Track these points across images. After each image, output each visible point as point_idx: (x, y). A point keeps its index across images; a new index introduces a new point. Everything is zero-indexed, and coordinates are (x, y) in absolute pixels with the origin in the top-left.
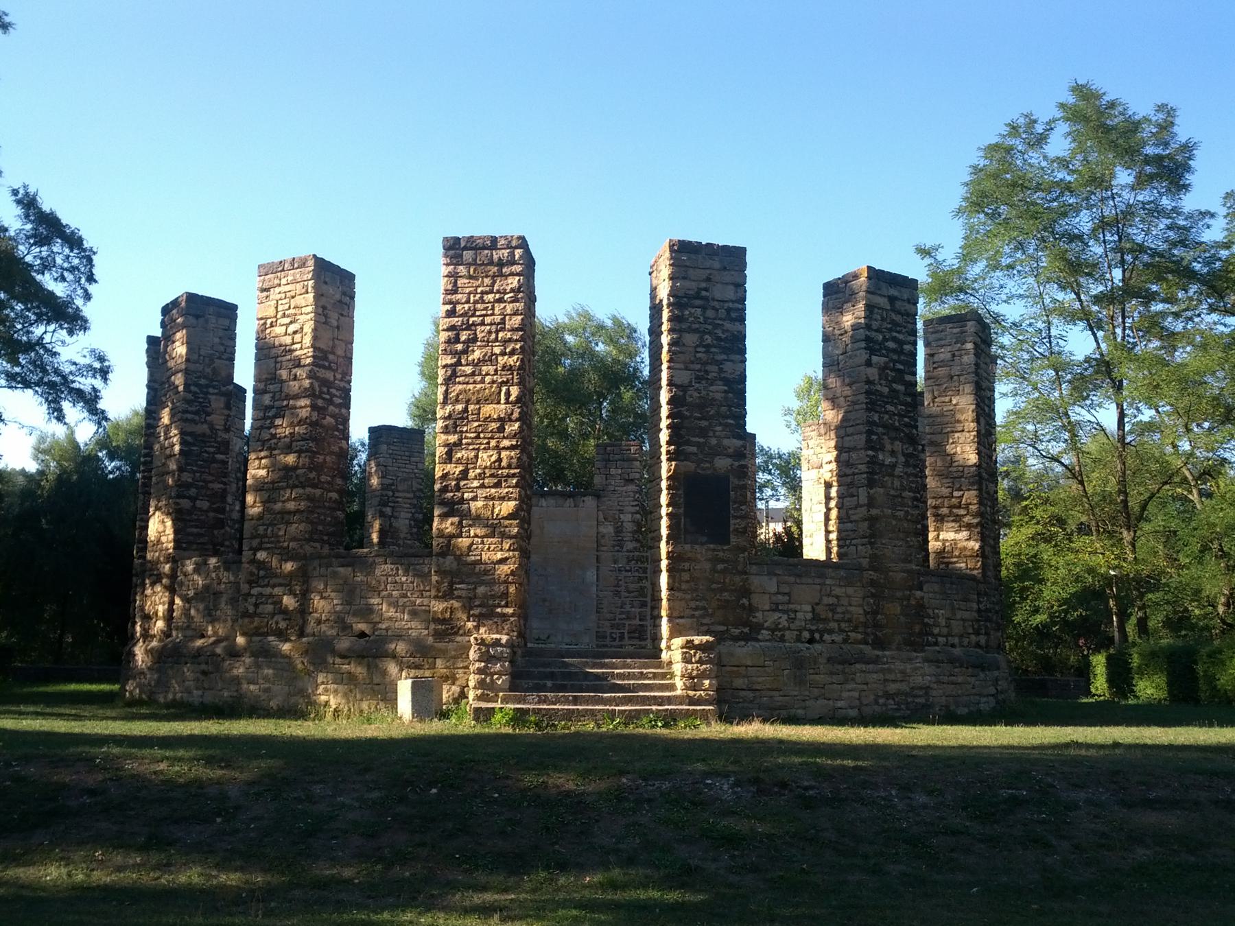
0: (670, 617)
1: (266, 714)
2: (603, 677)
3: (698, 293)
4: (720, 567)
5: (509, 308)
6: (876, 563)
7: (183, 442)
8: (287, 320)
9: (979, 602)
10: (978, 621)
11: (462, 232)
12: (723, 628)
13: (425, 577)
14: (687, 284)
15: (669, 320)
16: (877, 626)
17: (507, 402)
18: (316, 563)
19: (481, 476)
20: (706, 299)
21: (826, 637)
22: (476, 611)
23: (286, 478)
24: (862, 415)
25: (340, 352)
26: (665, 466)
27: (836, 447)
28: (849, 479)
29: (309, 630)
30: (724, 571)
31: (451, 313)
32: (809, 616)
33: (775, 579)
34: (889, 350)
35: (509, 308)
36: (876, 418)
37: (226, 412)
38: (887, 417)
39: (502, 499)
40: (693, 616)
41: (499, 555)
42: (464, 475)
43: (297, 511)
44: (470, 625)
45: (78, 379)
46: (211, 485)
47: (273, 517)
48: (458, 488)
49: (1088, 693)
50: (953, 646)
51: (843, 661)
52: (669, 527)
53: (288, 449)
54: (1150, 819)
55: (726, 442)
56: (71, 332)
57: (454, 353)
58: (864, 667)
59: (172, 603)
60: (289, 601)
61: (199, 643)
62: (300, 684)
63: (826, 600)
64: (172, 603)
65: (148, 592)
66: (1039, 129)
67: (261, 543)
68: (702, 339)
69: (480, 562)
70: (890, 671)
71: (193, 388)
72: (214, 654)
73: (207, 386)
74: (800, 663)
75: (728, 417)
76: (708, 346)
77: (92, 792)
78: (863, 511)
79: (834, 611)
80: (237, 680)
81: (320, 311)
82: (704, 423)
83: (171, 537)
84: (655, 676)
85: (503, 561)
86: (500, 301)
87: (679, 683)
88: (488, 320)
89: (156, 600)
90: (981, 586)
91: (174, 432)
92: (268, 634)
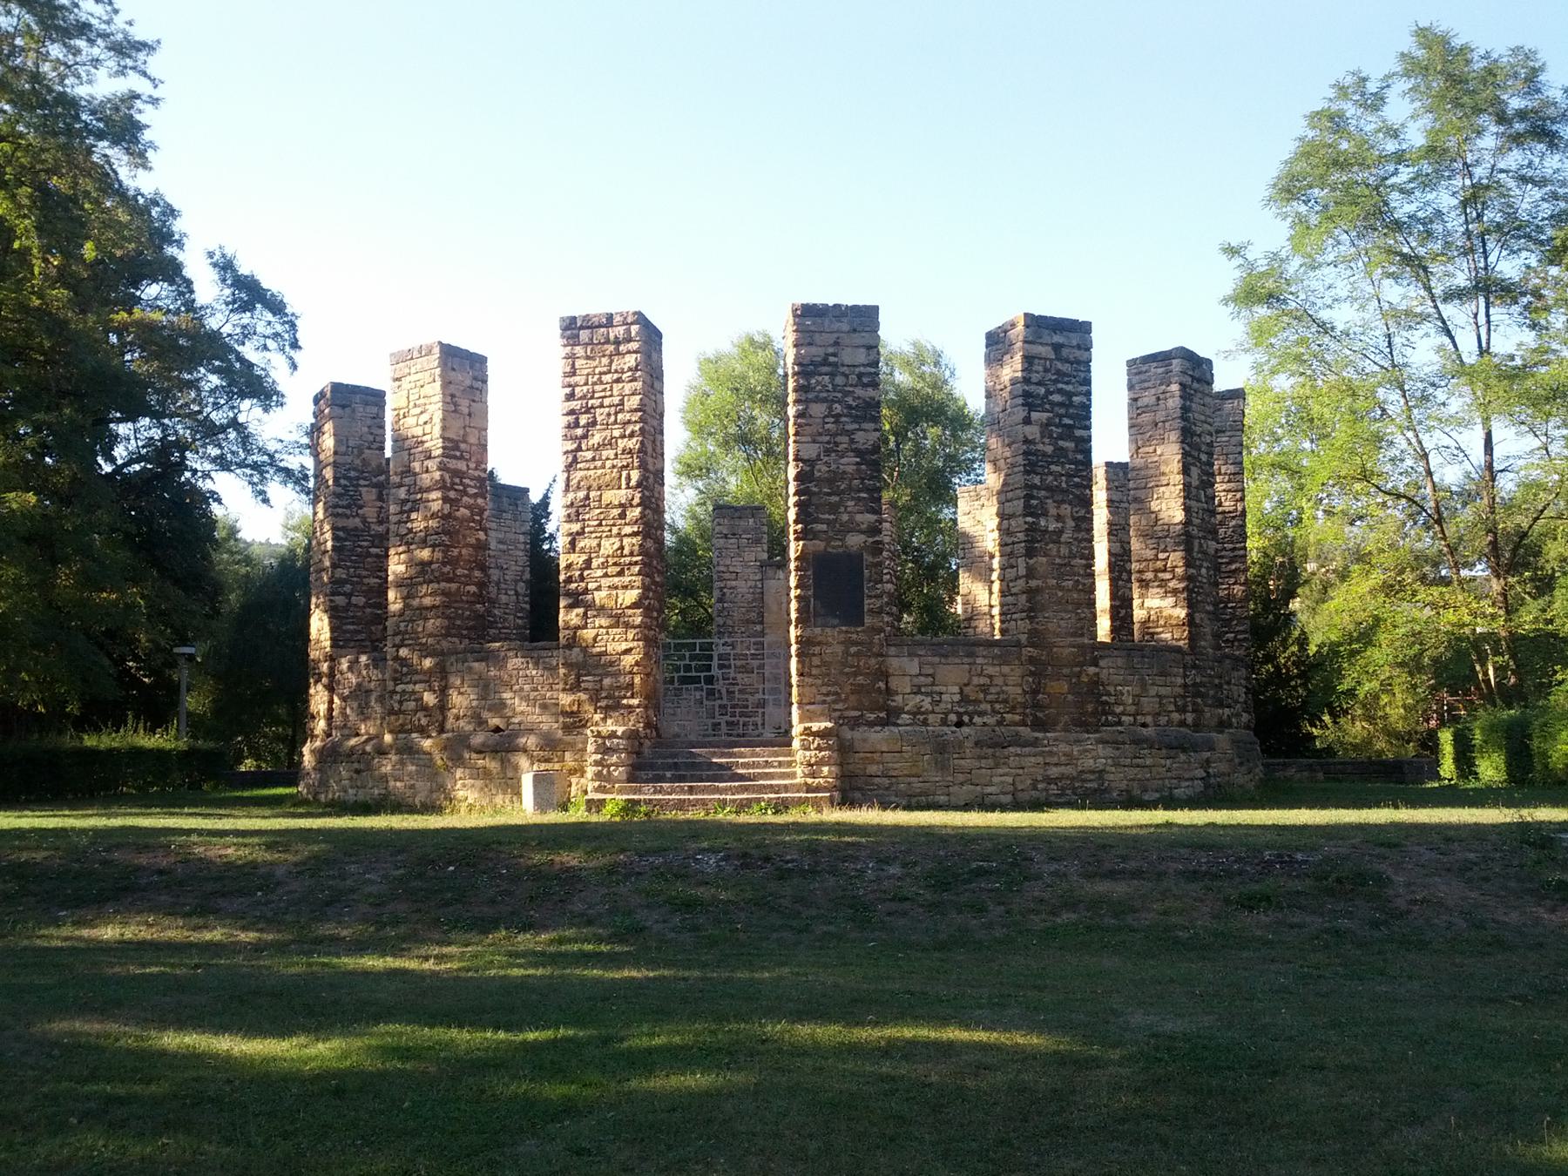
0: (800, 703)
1: (412, 810)
2: (728, 767)
3: (825, 359)
4: (853, 650)
5: (628, 388)
6: (1036, 638)
7: (335, 538)
8: (418, 410)
9: (1185, 676)
10: (1184, 697)
11: (579, 312)
12: (857, 713)
13: (553, 669)
14: (813, 350)
15: (795, 390)
16: (1037, 706)
17: (628, 487)
18: (453, 659)
19: (604, 565)
20: (835, 365)
21: (976, 719)
22: (603, 703)
23: (422, 572)
24: (1019, 479)
25: (472, 440)
26: (793, 545)
27: (998, 514)
28: (1008, 549)
29: (448, 726)
30: (857, 654)
31: (570, 397)
32: (957, 698)
33: (916, 660)
34: (1053, 404)
35: (628, 388)
36: (1037, 480)
37: (379, 504)
38: (1050, 478)
39: (625, 587)
40: (824, 702)
41: (624, 646)
42: (588, 564)
43: (434, 607)
44: (597, 717)
45: (285, 456)
46: (366, 581)
47: (414, 613)
48: (582, 578)
49: (1438, 777)
50: (1144, 725)
51: (994, 745)
52: (798, 610)
53: (424, 543)
54: (1102, 887)
55: (859, 517)
56: (266, 410)
57: (574, 438)
58: (1018, 750)
59: (331, 702)
60: (429, 698)
61: (353, 742)
62: (440, 780)
63: (976, 680)
64: (331, 702)
65: (312, 691)
66: (1372, 87)
67: (403, 640)
68: (830, 408)
69: (605, 653)
70: (1051, 753)
71: (343, 482)
72: (364, 752)
73: (358, 479)
74: (941, 748)
75: (860, 491)
76: (838, 416)
77: (161, 872)
78: (1021, 582)
79: (986, 692)
80: (384, 778)
81: (448, 399)
82: (835, 499)
83: (328, 635)
84: (780, 764)
85: (628, 651)
86: (618, 381)
87: (799, 770)
88: (607, 402)
89: (319, 699)
90: (1188, 658)
91: (327, 527)
92: (411, 731)
